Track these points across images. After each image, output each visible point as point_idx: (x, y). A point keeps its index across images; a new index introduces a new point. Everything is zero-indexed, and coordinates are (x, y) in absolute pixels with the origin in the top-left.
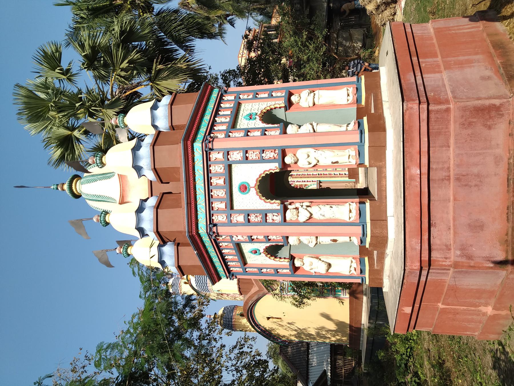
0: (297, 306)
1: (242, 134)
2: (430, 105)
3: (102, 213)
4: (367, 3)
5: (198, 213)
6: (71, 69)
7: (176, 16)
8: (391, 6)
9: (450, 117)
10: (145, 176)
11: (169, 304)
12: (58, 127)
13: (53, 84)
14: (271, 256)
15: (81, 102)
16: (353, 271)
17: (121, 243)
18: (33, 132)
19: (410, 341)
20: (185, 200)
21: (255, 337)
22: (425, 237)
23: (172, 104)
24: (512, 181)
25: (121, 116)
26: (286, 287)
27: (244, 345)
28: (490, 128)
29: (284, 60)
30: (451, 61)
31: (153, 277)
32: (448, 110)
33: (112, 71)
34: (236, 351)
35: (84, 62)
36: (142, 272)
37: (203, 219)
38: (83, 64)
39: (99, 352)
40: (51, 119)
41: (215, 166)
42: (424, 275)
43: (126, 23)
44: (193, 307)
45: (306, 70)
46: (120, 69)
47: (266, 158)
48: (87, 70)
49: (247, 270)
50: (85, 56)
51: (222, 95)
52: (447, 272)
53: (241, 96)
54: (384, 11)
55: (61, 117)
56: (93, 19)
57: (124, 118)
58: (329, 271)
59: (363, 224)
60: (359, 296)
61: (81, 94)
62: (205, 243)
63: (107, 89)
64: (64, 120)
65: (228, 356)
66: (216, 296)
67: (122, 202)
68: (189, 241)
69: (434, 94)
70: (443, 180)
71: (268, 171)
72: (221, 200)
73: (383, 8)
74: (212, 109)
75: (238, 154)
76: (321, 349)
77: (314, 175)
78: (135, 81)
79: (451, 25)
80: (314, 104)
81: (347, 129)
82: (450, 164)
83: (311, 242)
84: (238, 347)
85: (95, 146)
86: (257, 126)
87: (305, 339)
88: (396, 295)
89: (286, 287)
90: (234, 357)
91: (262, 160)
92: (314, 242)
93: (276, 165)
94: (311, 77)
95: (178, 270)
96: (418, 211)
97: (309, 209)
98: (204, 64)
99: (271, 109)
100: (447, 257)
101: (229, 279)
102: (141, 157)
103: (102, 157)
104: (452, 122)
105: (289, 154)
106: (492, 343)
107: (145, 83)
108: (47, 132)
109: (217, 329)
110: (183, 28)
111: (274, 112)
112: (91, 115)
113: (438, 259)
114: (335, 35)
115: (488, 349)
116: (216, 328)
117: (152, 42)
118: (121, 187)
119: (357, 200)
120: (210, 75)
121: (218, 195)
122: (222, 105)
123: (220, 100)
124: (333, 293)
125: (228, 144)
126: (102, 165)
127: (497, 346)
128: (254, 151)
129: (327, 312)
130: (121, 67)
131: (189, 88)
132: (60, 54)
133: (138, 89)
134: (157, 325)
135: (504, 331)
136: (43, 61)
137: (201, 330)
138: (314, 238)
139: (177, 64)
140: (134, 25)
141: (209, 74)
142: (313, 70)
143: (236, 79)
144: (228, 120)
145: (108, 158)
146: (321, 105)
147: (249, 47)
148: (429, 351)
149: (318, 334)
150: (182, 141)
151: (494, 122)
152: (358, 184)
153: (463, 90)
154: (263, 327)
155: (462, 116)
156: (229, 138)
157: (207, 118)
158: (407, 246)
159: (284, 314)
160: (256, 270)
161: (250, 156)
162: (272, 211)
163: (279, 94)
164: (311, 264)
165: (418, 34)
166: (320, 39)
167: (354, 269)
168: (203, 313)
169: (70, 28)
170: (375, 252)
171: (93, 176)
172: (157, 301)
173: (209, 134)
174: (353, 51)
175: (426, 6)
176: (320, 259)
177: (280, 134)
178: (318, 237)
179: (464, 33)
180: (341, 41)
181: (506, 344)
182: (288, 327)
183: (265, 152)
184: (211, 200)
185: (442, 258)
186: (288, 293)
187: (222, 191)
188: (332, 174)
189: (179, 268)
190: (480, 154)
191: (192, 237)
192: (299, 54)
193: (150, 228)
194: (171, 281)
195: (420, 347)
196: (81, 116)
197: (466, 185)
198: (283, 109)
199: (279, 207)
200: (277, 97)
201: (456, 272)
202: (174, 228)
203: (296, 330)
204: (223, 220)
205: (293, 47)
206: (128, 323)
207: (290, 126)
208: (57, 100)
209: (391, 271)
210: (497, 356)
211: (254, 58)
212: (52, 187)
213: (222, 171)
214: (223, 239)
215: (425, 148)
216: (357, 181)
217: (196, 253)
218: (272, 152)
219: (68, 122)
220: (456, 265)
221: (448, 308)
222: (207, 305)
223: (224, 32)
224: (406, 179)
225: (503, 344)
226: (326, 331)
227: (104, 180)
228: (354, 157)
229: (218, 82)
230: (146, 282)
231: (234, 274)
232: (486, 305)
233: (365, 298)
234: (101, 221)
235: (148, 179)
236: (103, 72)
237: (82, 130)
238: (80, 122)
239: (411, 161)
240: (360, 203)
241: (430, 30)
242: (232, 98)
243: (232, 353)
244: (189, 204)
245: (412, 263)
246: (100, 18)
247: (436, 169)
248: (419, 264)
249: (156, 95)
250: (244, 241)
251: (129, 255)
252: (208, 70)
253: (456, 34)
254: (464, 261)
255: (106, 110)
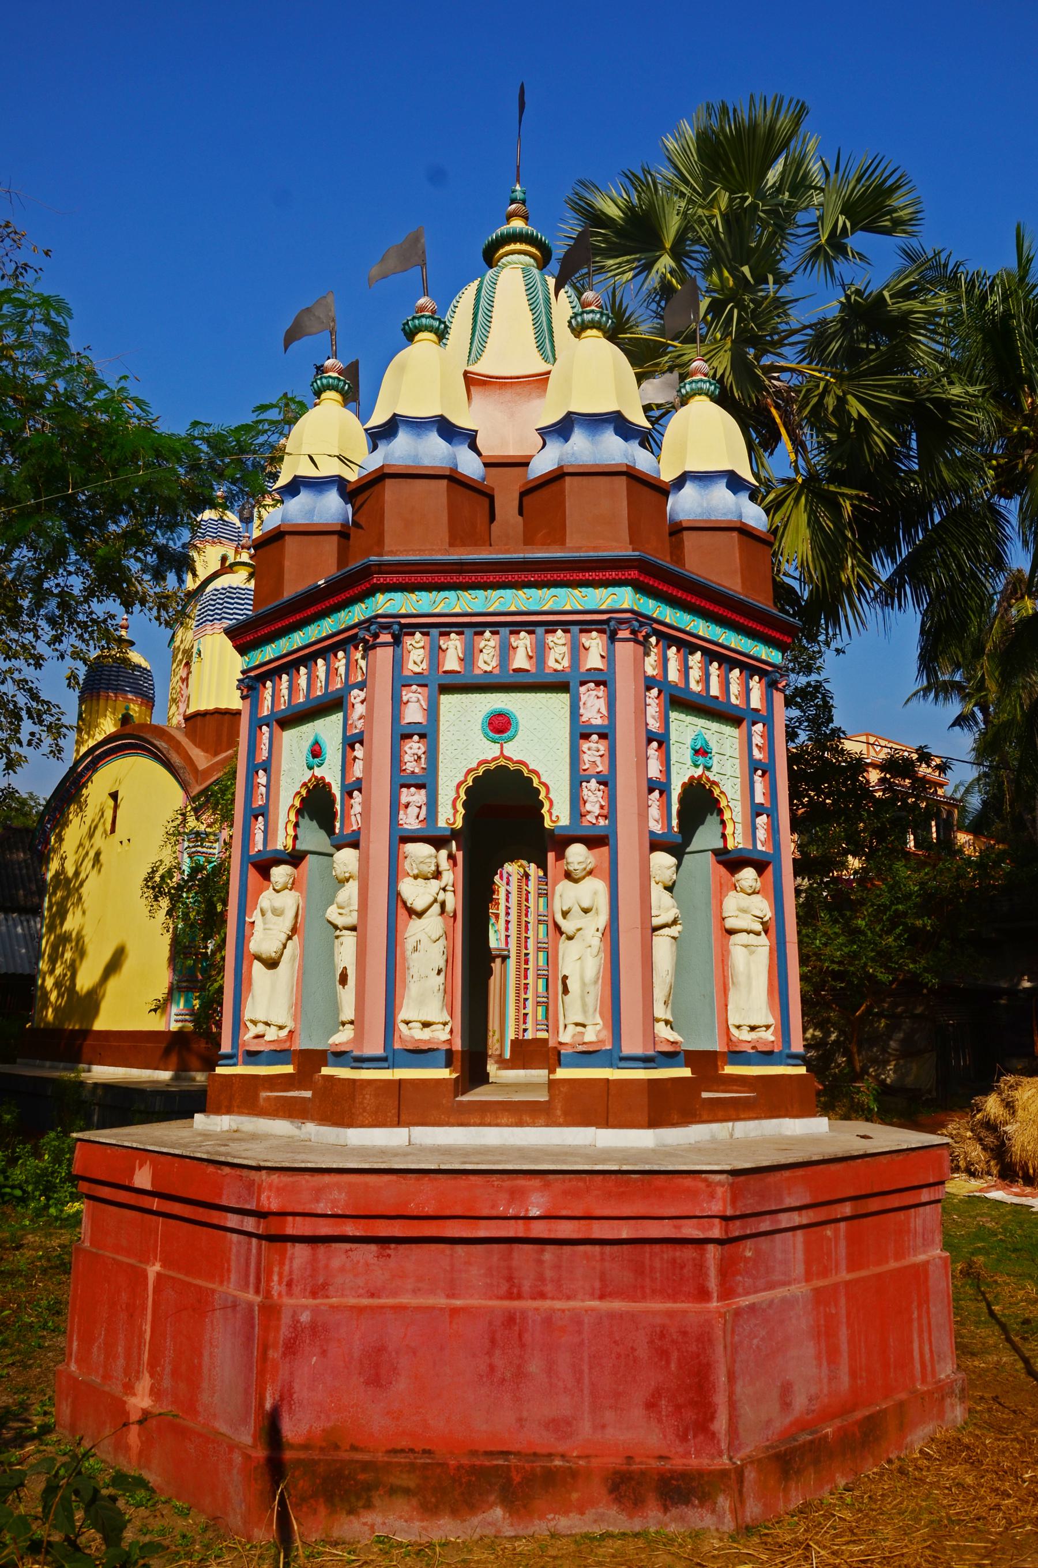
0: (150, 877)
1: (654, 725)
2: (719, 1247)
3: (441, 322)
4: (1004, 1096)
5: (435, 593)
6: (847, 259)
7: (985, 560)
8: (992, 1163)
9: (683, 1301)
10: (543, 447)
11: (170, 506)
12: (685, 214)
13: (803, 206)
14: (303, 801)
15: (752, 282)
16: (253, 1031)
17: (352, 372)
18: (671, 144)
19: (43, 1198)
20: (471, 557)
21: (63, 755)
22: (350, 1229)
23: (744, 531)
24: (501, 1462)
25: (713, 387)
26: (204, 850)
27: (41, 722)
28: (651, 1405)
29: (854, 863)
30: (836, 1306)
31: (249, 463)
32: (703, 1295)
33: (838, 371)
34: (22, 700)
35: (866, 294)
36: (266, 431)
37: (416, 605)
38: (858, 293)
39: (46, 302)
40: (708, 196)
41: (564, 645)
42: (242, 1221)
43: (970, 417)
44: (159, 576)
45: (826, 924)
46: (845, 394)
47: (585, 791)
48: (841, 302)
49: (265, 729)
50: (880, 297)
51: (762, 674)
52: (251, 1286)
53: (759, 727)
54: (981, 1144)
55: (714, 222)
56: (981, 330)
57: (706, 394)
58: (257, 964)
59: (390, 1059)
60: (174, 1059)
61: (774, 283)
62: (347, 610)
63: (789, 356)
64: (702, 231)
65: (8, 675)
66: (182, 647)
67: (471, 381)
68: (355, 564)
69: (749, 1258)
70: (510, 1279)
71: (547, 797)
72: (469, 657)
73: (990, 1140)
74: (726, 643)
75: (599, 711)
76: (19, 946)
77: (526, 942)
78: (808, 436)
79: (933, 1310)
80: (731, 932)
81: (658, 1020)
82: (553, 1298)
83: (341, 911)
84: (34, 704)
85: (627, 315)
86: (674, 770)
87: (50, 901)
88: (185, 1146)
89: (204, 850)
90: (5, 694)
91: (578, 779)
92: (340, 921)
93: (565, 821)
94: (806, 939)
95: (270, 531)
96: (423, 1208)
97: (436, 908)
98: (850, 634)
99: (721, 812)
100: (294, 1286)
101: (241, 676)
102: (597, 437)
103: (599, 328)
104: (670, 1305)
105: (595, 857)
106: (46, 1408)
107: (801, 463)
108: (671, 181)
109: (88, 645)
110: (952, 578)
111: (712, 820)
112: (716, 308)
113: (287, 1262)
114: (919, 1010)
115: (28, 1398)
116: (91, 642)
117: (915, 488)
118: (511, 378)
119: (458, 1046)
120: (820, 652)
121: (481, 651)
122: (736, 672)
123: (751, 668)
124: (185, 984)
125: (625, 685)
126: (578, 330)
127: (39, 1423)
128: (606, 759)
129: (128, 966)
130: (850, 397)
131: (783, 588)
132: (887, 232)
133: (786, 442)
134: (115, 470)
135: (81, 1439)
136: (868, 183)
137: (87, 600)
138: (352, 919)
139: (854, 557)
140: (963, 439)
141: (823, 649)
142: (825, 945)
143: (806, 724)
144: (695, 687)
145: (596, 343)
146: (728, 952)
147: (895, 766)
148: (17, 1248)
149: (64, 939)
150: (637, 553)
151: (667, 1416)
152: (496, 1066)
153: (755, 1337)
154: (90, 779)
155: (684, 1333)
156: (643, 687)
157: (702, 628)
158: (327, 1179)
159: (125, 842)
160: (265, 754)
161: (592, 745)
162: (432, 804)
163: (761, 834)
164: (278, 912)
165: (912, 1220)
166: (911, 966)
167: (261, 1033)
168: (137, 607)
169: (957, 265)
170: (308, 1094)
171: (548, 301)
172: (181, 471)
173: (656, 633)
174: (874, 1061)
175: (987, 1254)
176: (290, 938)
177: (652, 833)
178: (354, 933)
179: (911, 1342)
180: (904, 1027)
181: (46, 1445)
182: (87, 853)
183: (602, 787)
184: (469, 632)
185: (291, 1272)
186: (186, 855)
187: (494, 663)
188: (526, 993)
189: (276, 537)
190: (579, 1381)
191: (367, 571)
192: (872, 906)
193: (397, 455)
194: (232, 517)
195: (27, 1223)
196: (715, 278)
197: (493, 1341)
198: (720, 844)
199: (442, 823)
200: (754, 828)
201: (251, 1310)
202: (391, 524)
203: (77, 874)
204: (411, 663)
205: (891, 888)
206: (122, 388)
207: (672, 860)
208: (762, 214)
209: (254, 1137)
210: (11, 1420)
211: (863, 777)
212: (518, 188)
213: (551, 663)
214: (357, 661)
215: (599, 1230)
216: (504, 1064)
217: (320, 583)
218: (602, 807)
219: (697, 241)
220: (270, 1311)
221: (146, 1289)
222: (158, 618)
223: (941, 697)
224: (515, 1179)
225: (44, 1438)
226: (73, 961)
227: (532, 317)
228: (578, 1039)
229: (798, 673)
230: (238, 441)
231: (255, 693)
232: (155, 1393)
233: (165, 1075)
234: (419, 318)
235: (532, 457)
236: (835, 346)
237: (674, 281)
238: (699, 277)
239: (565, 1193)
240: (449, 1053)
241: (925, 1252)
242: (756, 702)
243: (16, 688)
244: (461, 567)
245: (278, 1189)
246: (984, 347)
247: (540, 1262)
248: (274, 1207)
249: (768, 493)
250: (350, 722)
251: (318, 394)
252: (833, 646)
253: (910, 1321)
254: (281, 1333)
255: (730, 350)
